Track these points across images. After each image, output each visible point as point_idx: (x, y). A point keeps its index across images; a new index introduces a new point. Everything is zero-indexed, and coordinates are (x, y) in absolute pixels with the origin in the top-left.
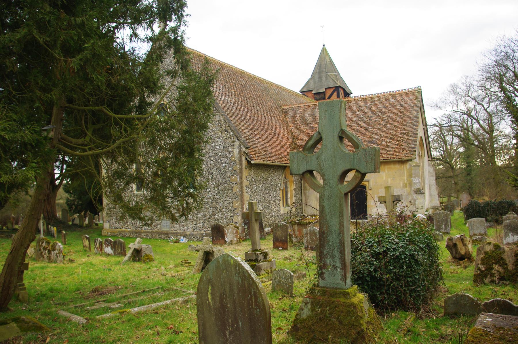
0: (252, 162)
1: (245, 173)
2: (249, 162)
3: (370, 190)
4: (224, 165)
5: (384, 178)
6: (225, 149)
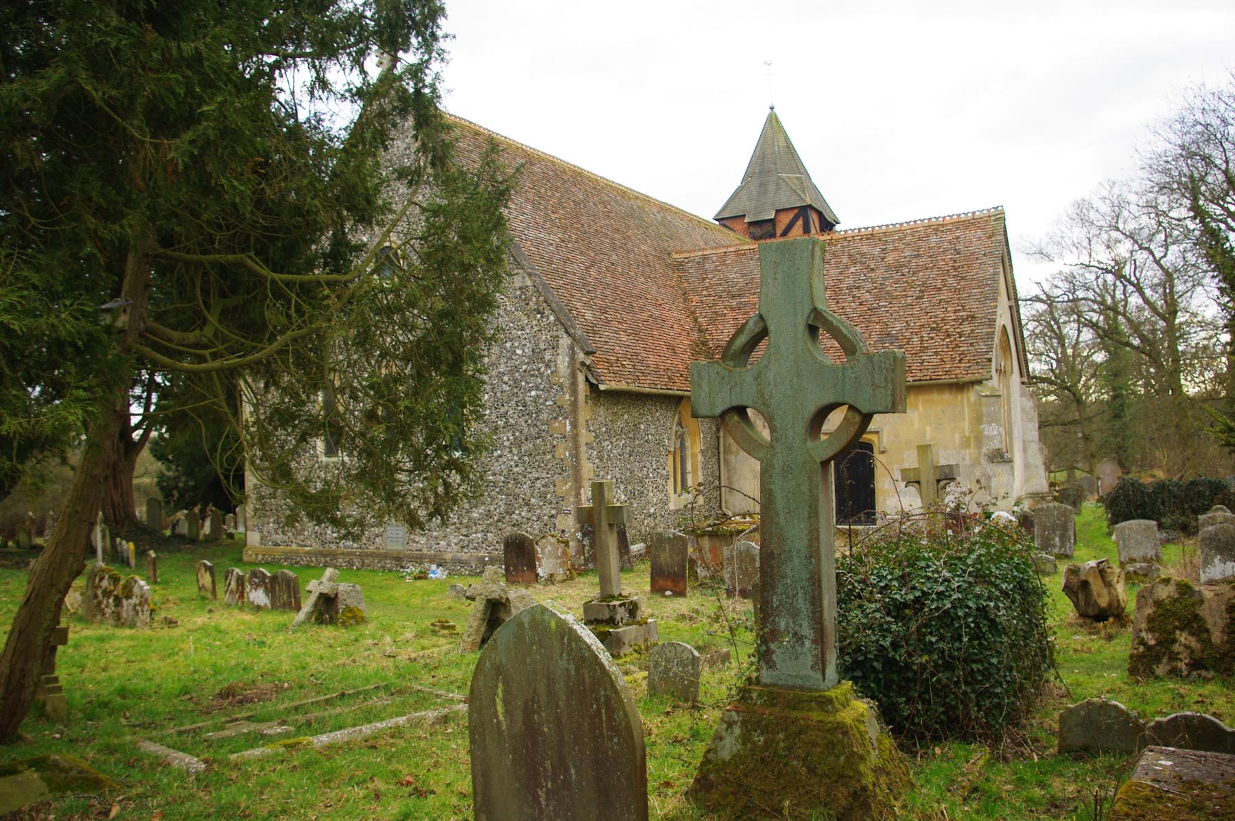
0: (602, 387)
1: (584, 414)
2: (593, 388)
3: (883, 452)
4: (533, 393)
5: (917, 425)
6: (537, 355)
